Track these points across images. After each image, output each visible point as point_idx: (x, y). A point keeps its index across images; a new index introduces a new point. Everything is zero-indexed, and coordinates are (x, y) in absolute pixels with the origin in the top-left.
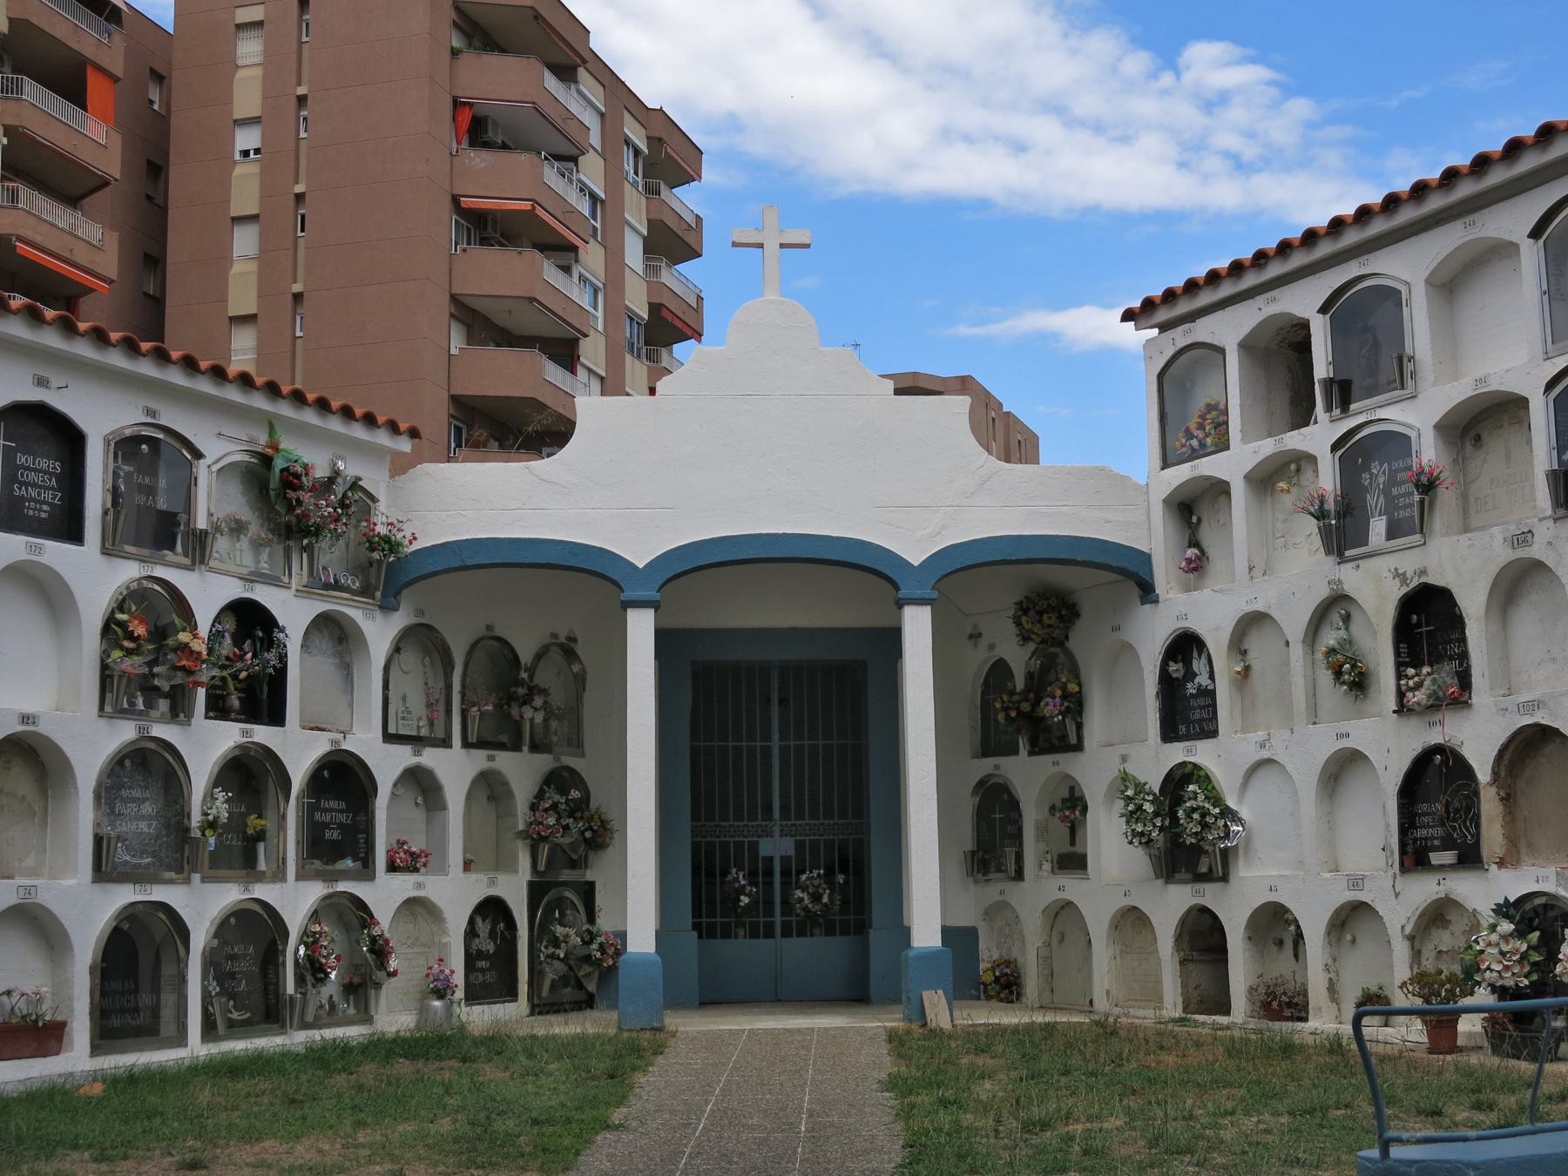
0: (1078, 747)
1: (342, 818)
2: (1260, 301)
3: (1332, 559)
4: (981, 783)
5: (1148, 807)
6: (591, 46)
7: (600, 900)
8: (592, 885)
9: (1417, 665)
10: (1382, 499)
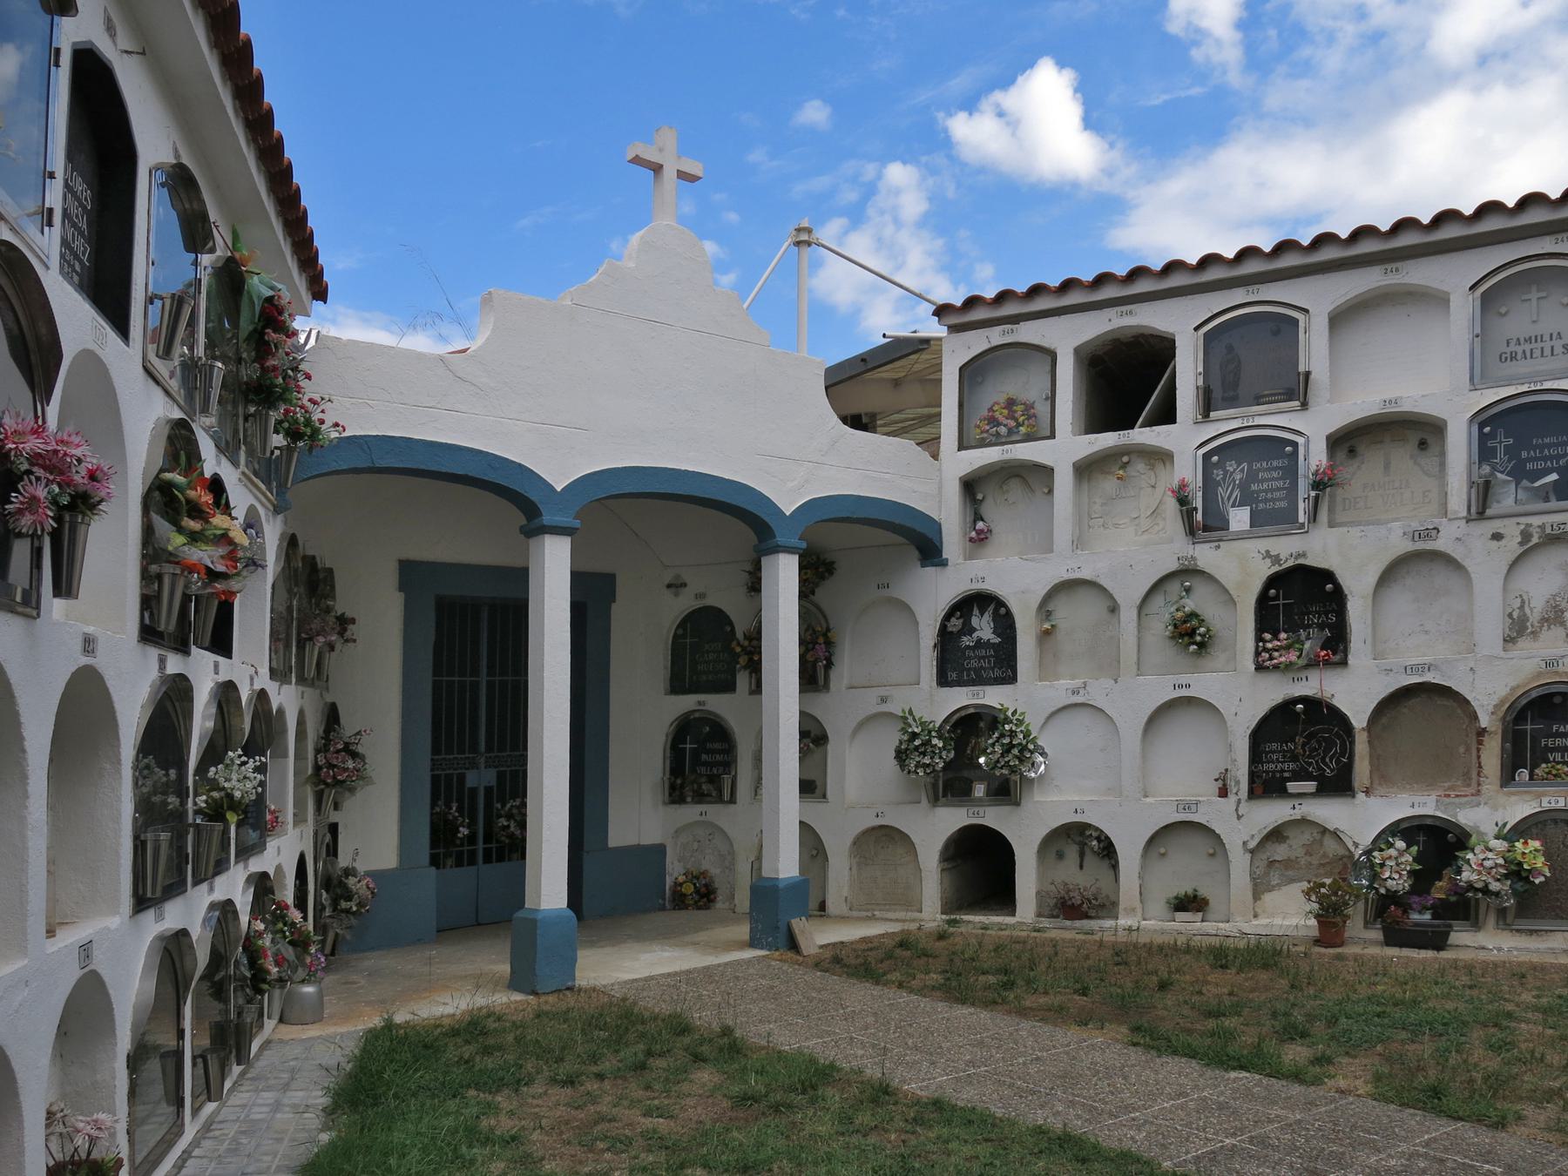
2: (1111, 313)
10: (1237, 492)
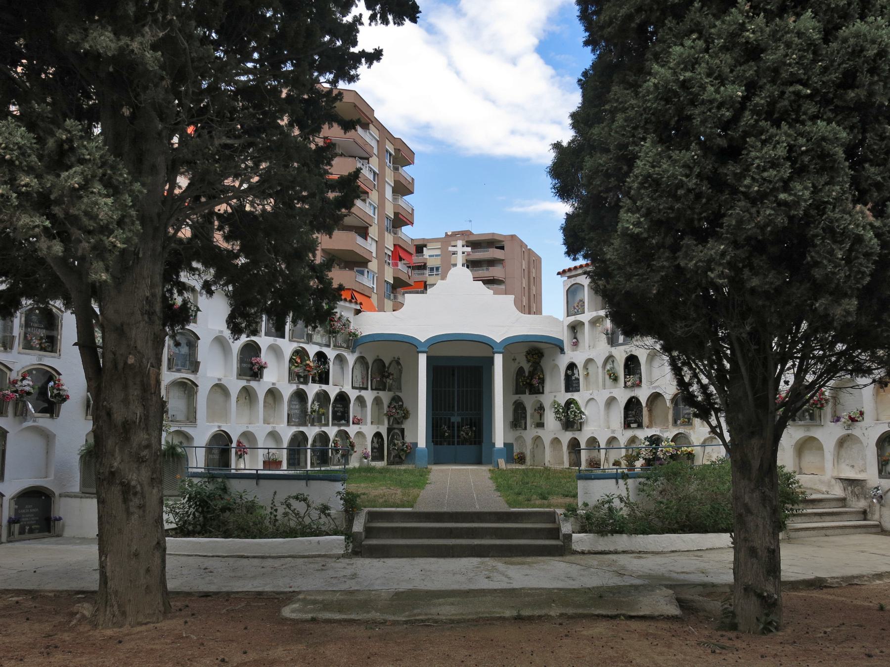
0: (543, 393)
1: (342, 409)
3: (609, 346)
4: (515, 402)
5: (561, 410)
6: (375, 116)
8: (404, 429)
9: (630, 375)
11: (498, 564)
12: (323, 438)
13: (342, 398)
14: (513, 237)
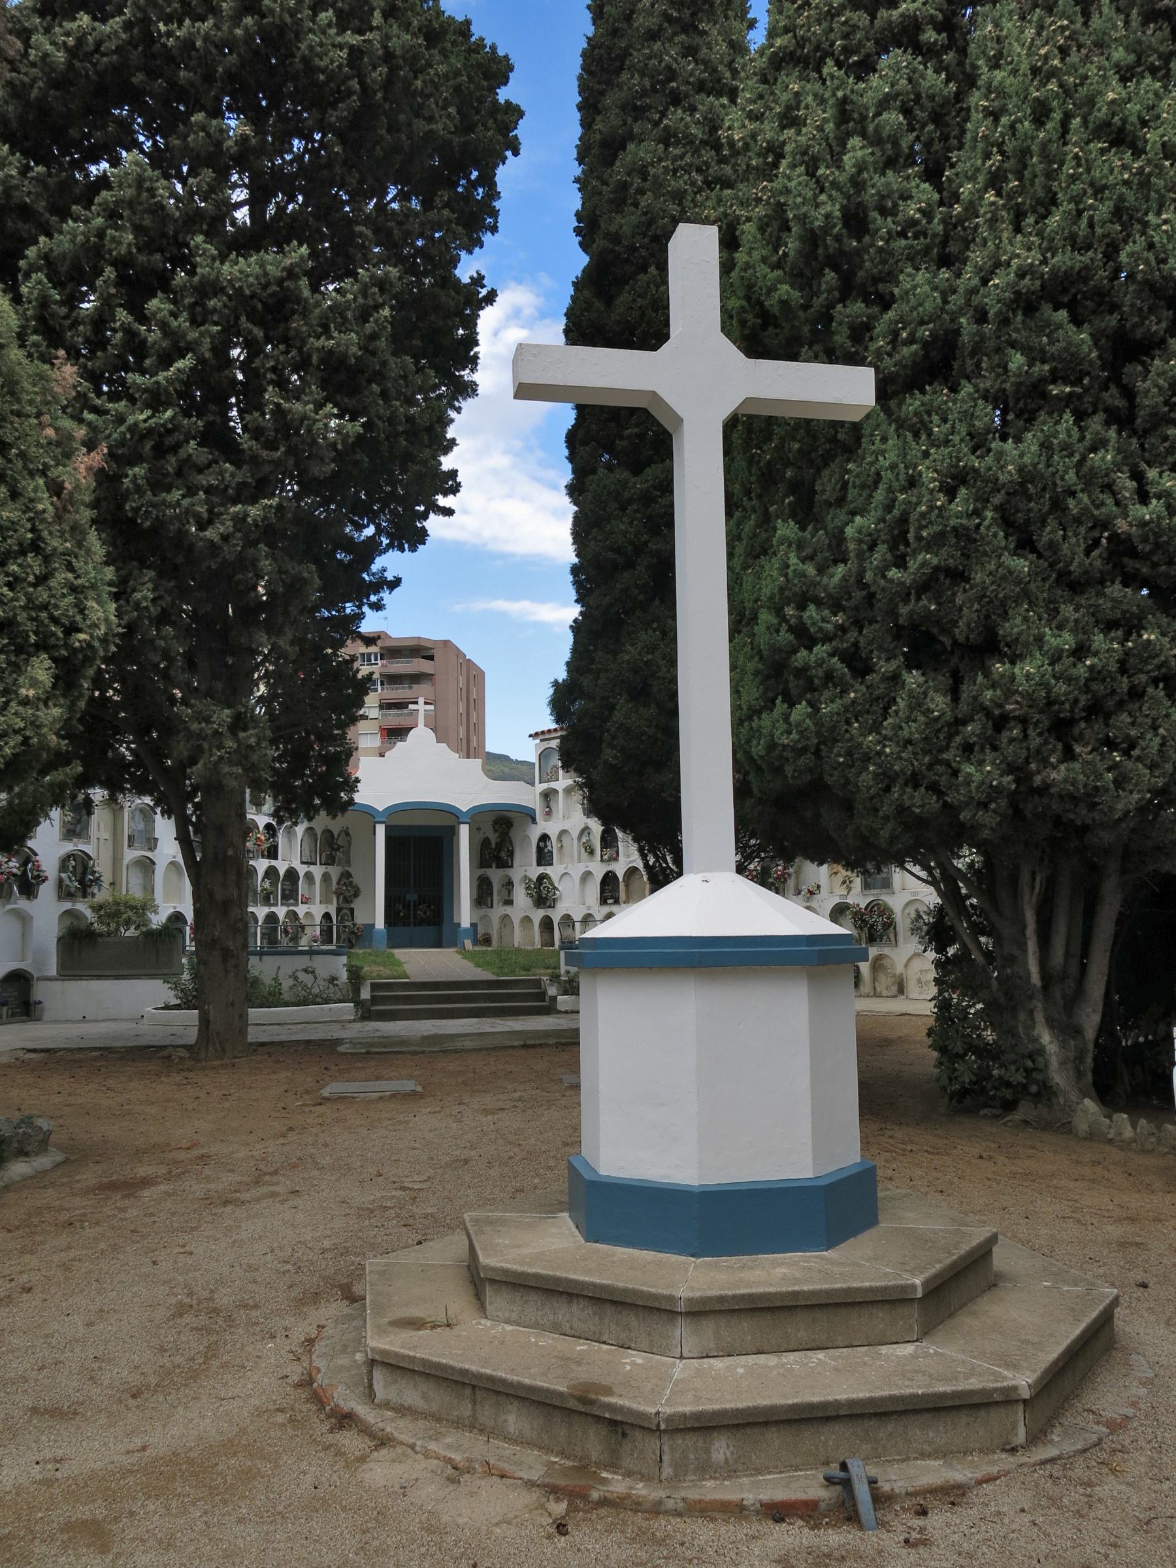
0: (512, 866)
7: (356, 913)
11: (497, 1021)
12: (271, 918)
13: (292, 874)
14: (446, 643)
